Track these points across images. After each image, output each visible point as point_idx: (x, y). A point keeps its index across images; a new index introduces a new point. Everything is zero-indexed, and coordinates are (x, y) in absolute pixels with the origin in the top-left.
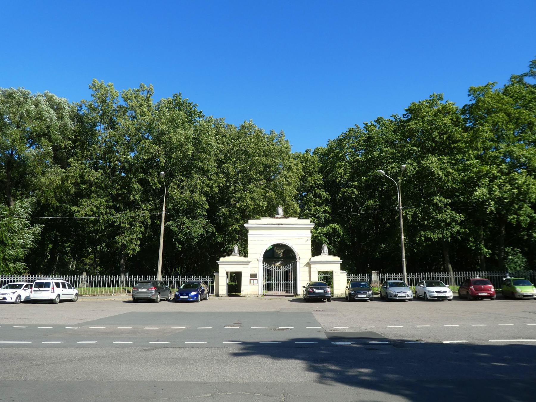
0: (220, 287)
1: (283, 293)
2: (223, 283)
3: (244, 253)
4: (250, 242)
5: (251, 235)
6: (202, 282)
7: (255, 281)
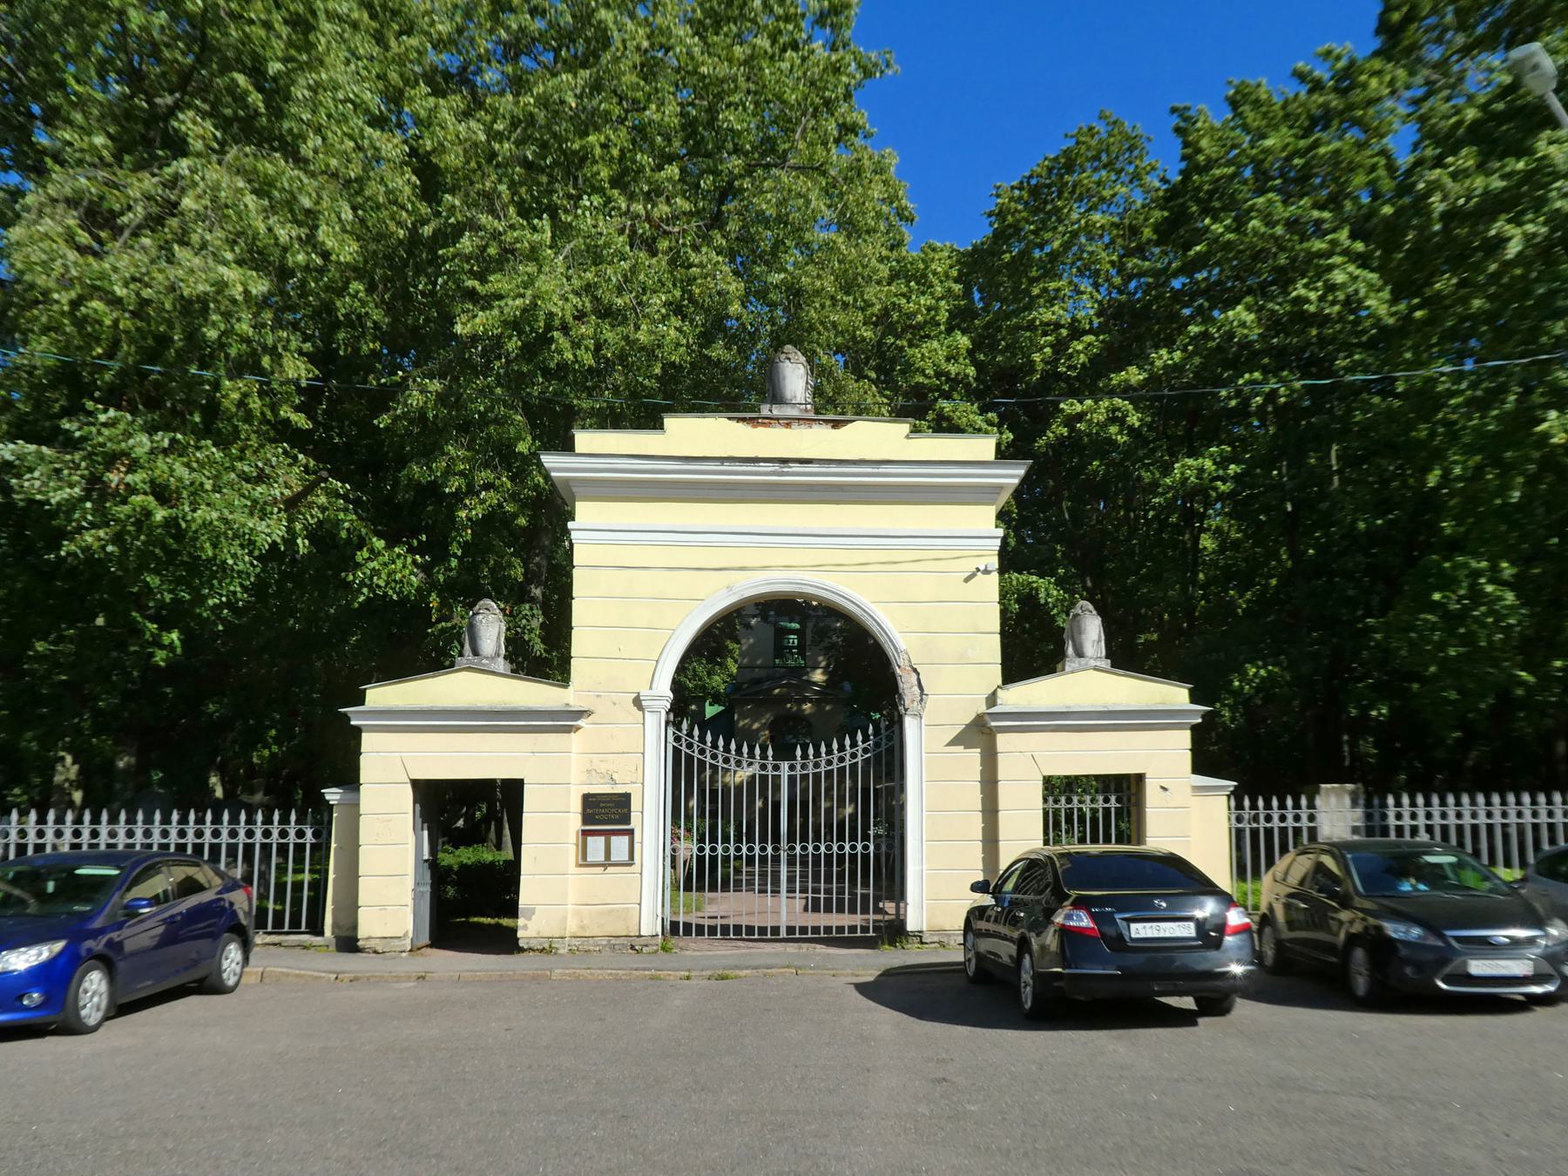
0: (363, 883)
1: (786, 909)
3: (543, 654)
4: (582, 583)
5: (594, 530)
6: (219, 841)
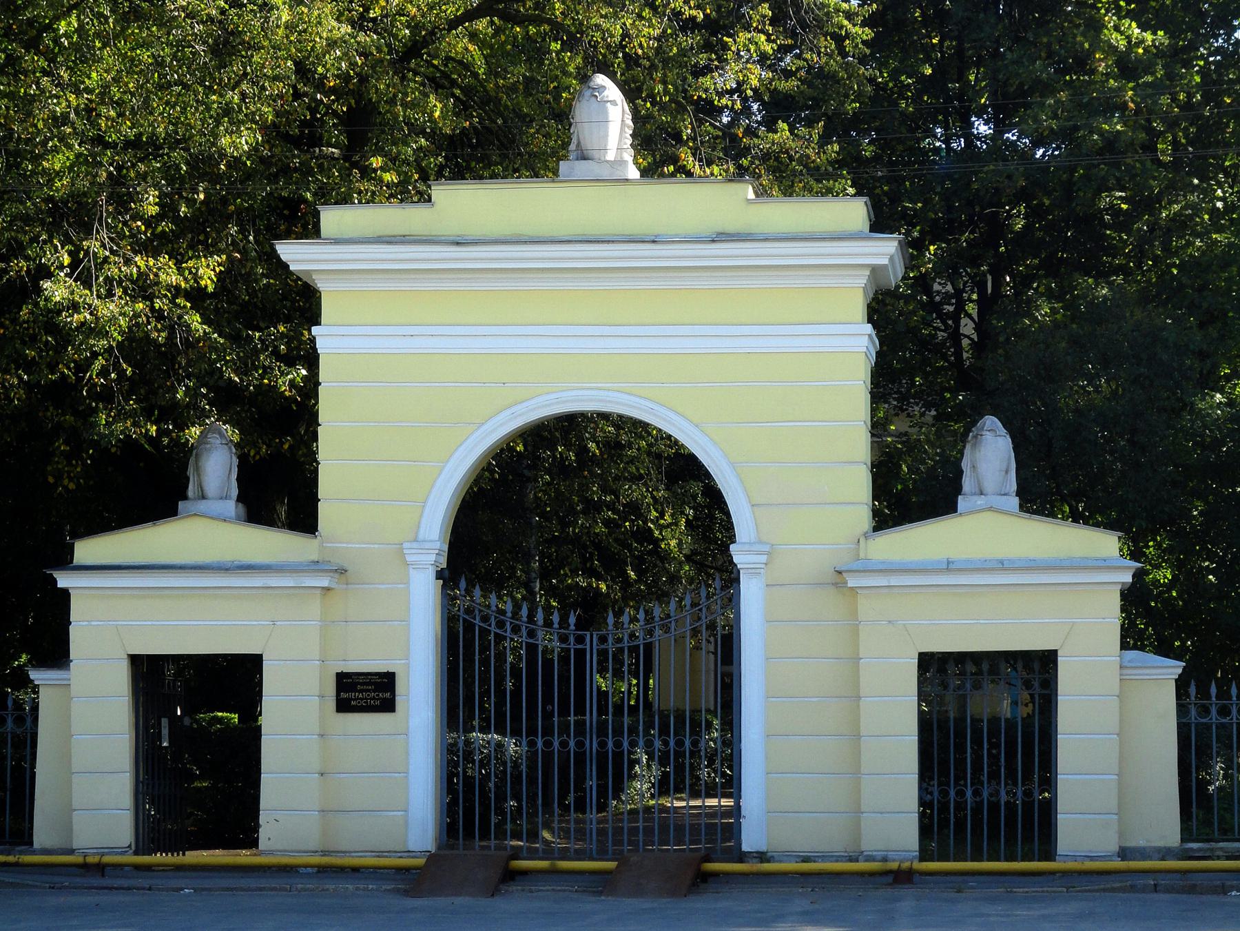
3: (282, 489)
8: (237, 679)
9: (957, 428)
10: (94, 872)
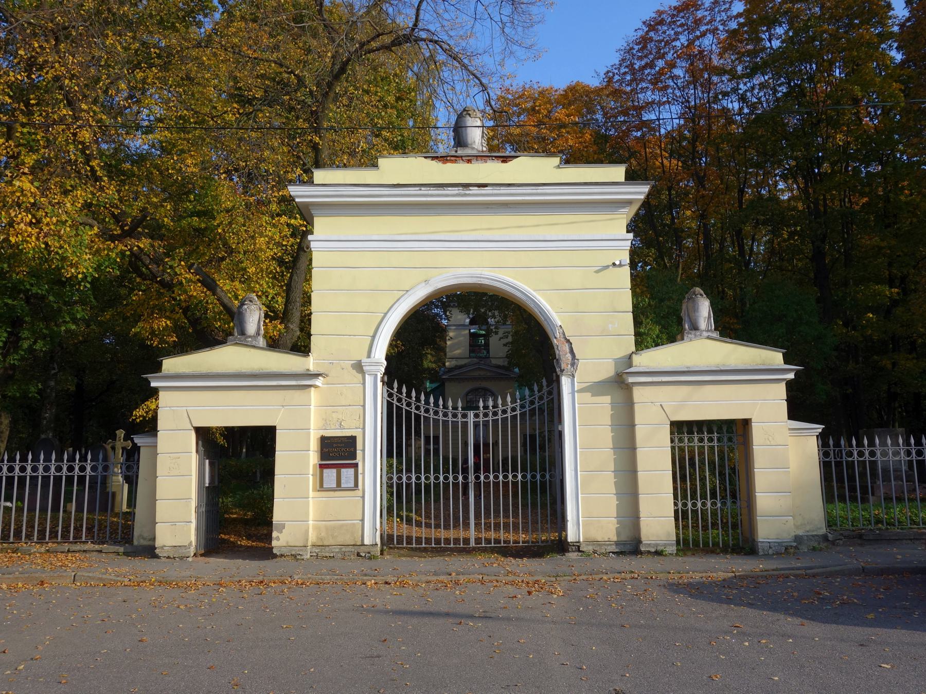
2: (176, 489)
7: (347, 473)
8: (261, 441)
9: (683, 294)
10: (178, 557)
